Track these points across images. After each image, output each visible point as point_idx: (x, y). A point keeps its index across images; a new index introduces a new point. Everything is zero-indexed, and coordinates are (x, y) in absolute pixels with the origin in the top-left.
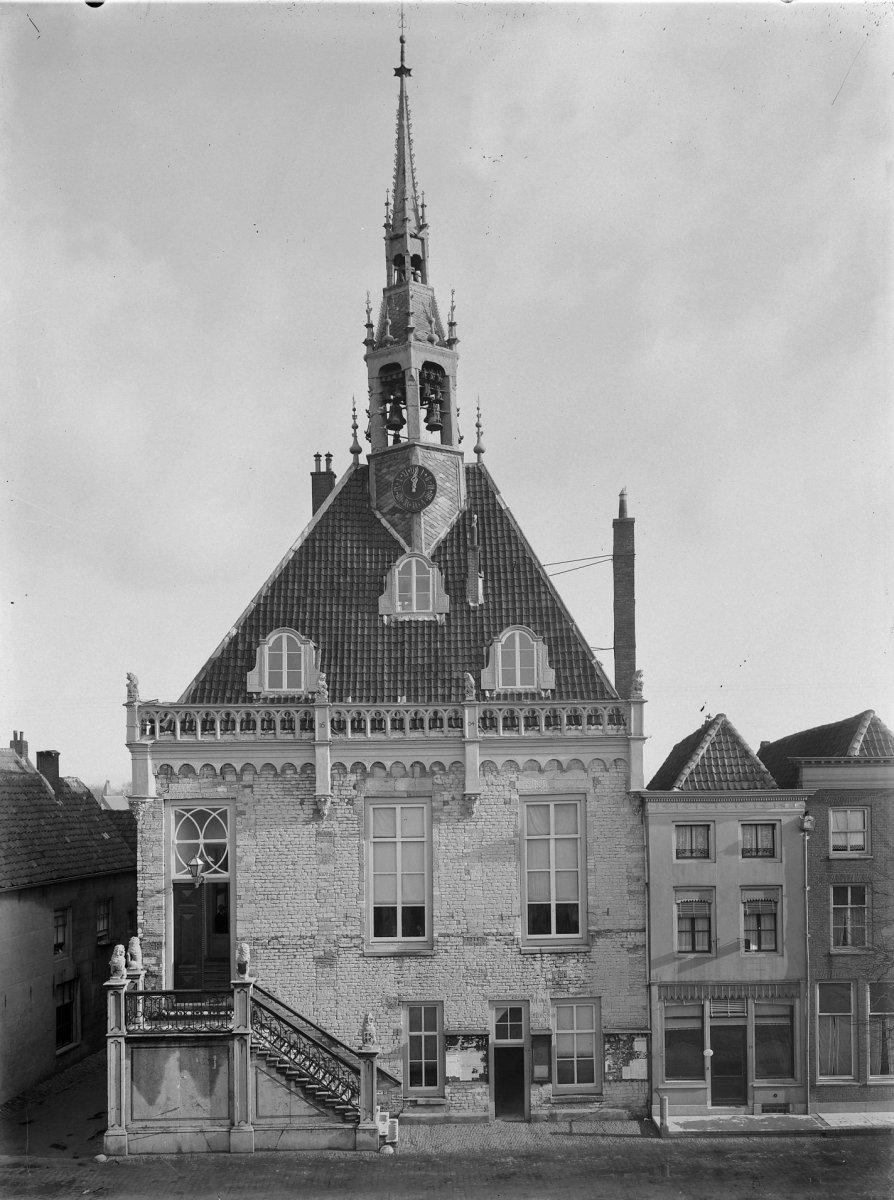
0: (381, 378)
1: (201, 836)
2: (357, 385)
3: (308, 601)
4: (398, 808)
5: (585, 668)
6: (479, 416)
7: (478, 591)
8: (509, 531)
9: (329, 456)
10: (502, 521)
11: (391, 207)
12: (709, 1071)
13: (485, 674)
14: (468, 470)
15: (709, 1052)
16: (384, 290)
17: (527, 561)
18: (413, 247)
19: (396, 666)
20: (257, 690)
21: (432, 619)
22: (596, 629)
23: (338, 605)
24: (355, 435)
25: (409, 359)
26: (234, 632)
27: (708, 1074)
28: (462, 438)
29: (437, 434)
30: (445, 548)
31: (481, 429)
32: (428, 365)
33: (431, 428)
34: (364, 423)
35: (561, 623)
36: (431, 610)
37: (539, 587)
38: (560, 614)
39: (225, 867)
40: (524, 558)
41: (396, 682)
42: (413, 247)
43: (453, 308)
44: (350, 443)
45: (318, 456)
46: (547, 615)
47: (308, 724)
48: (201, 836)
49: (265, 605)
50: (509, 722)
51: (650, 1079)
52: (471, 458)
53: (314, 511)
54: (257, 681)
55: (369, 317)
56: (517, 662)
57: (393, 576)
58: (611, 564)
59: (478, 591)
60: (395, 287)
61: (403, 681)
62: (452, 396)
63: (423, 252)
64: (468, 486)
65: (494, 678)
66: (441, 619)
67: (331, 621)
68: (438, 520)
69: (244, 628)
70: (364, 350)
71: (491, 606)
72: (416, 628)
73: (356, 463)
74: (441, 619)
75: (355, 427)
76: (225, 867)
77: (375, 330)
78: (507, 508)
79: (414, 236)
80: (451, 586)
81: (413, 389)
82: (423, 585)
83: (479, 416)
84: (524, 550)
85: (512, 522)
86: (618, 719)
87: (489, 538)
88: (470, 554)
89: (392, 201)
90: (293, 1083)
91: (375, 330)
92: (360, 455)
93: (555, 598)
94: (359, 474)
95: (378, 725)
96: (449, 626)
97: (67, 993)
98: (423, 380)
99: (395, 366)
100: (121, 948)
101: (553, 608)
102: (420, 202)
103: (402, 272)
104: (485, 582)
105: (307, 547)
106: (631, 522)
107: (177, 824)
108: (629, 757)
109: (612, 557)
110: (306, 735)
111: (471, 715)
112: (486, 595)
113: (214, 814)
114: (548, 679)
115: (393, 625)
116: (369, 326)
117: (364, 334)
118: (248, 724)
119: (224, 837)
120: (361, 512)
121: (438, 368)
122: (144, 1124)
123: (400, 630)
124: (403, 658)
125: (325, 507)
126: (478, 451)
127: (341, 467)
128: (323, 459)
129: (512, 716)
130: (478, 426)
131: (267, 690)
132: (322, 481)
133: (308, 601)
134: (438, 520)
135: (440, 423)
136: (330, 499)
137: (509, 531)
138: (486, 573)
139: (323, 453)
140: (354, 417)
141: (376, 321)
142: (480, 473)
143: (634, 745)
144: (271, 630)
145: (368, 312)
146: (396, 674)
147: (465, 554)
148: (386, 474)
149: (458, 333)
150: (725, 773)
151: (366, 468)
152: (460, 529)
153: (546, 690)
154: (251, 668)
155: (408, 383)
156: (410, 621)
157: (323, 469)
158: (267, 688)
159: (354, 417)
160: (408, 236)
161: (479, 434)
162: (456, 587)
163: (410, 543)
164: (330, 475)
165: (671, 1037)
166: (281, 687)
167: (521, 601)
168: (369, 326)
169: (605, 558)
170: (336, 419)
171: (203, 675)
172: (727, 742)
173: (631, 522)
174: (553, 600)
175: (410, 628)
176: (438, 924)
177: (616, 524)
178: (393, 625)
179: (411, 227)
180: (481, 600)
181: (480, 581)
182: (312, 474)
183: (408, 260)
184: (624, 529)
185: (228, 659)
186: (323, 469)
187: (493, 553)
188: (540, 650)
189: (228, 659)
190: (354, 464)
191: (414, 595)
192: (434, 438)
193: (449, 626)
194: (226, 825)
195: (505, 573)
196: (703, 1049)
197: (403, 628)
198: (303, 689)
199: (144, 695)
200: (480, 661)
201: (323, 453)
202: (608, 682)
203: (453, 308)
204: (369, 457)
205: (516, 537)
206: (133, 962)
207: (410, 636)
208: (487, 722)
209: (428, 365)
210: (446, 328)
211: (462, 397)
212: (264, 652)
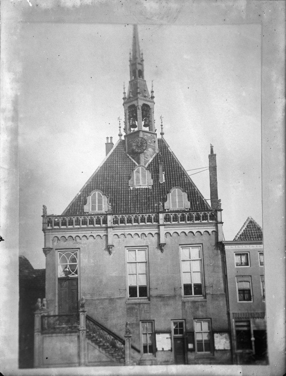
0: (129, 110)
1: (68, 262)
2: (120, 112)
6: (162, 122)
8: (173, 159)
9: (111, 138)
10: (170, 156)
11: (131, 55)
13: (166, 204)
14: (159, 140)
15: (253, 339)
17: (180, 168)
18: (139, 67)
19: (135, 203)
21: (147, 187)
24: (120, 130)
26: (80, 193)
27: (253, 347)
28: (156, 130)
30: (151, 165)
31: (163, 127)
32: (144, 105)
33: (145, 126)
34: (123, 126)
35: (192, 187)
37: (184, 176)
38: (191, 184)
39: (76, 273)
40: (178, 167)
41: (135, 208)
42: (139, 67)
43: (152, 86)
44: (118, 132)
45: (108, 138)
48: (68, 262)
50: (175, 219)
52: (159, 136)
53: (107, 153)
54: (87, 208)
56: (177, 200)
64: (158, 143)
65: (169, 205)
66: (150, 187)
67: (113, 189)
71: (167, 183)
72: (142, 190)
73: (120, 139)
74: (150, 187)
75: (120, 127)
76: (76, 273)
79: (139, 64)
81: (139, 112)
82: (144, 176)
83: (162, 122)
84: (178, 165)
85: (174, 156)
86: (214, 217)
89: (132, 53)
95: (130, 221)
98: (143, 110)
101: (189, 182)
102: (141, 53)
103: (135, 77)
104: (165, 175)
107: (59, 258)
110: (104, 225)
111: (161, 216)
112: (166, 179)
114: (188, 205)
115: (134, 190)
116: (124, 93)
117: (123, 96)
118: (84, 223)
121: (147, 106)
124: (137, 200)
129: (175, 217)
130: (162, 126)
131: (91, 211)
132: (109, 145)
133: (105, 183)
136: (112, 151)
137: (173, 159)
138: (165, 172)
139: (109, 137)
140: (120, 124)
141: (127, 91)
142: (163, 141)
145: (124, 88)
146: (135, 205)
147: (158, 166)
149: (154, 94)
150: (253, 235)
151: (124, 141)
153: (187, 209)
154: (85, 204)
155: (138, 110)
156: (140, 188)
157: (109, 142)
158: (91, 211)
160: (137, 64)
161: (162, 128)
162: (156, 177)
168: (124, 93)
169: (205, 169)
171: (69, 207)
172: (252, 225)
174: (189, 180)
175: (140, 190)
178: (134, 190)
179: (139, 61)
180: (164, 181)
181: (163, 175)
182: (106, 144)
184: (212, 157)
185: (78, 202)
186: (109, 142)
187: (169, 170)
188: (185, 195)
189: (78, 202)
192: (147, 129)
194: (77, 257)
196: (250, 337)
197: (137, 190)
198: (103, 210)
199: (49, 213)
200: (165, 200)
201: (109, 137)
202: (209, 206)
203: (152, 86)
204: (125, 136)
205: (175, 161)
208: (167, 219)
209: (144, 105)
211: (156, 116)
212: (89, 199)
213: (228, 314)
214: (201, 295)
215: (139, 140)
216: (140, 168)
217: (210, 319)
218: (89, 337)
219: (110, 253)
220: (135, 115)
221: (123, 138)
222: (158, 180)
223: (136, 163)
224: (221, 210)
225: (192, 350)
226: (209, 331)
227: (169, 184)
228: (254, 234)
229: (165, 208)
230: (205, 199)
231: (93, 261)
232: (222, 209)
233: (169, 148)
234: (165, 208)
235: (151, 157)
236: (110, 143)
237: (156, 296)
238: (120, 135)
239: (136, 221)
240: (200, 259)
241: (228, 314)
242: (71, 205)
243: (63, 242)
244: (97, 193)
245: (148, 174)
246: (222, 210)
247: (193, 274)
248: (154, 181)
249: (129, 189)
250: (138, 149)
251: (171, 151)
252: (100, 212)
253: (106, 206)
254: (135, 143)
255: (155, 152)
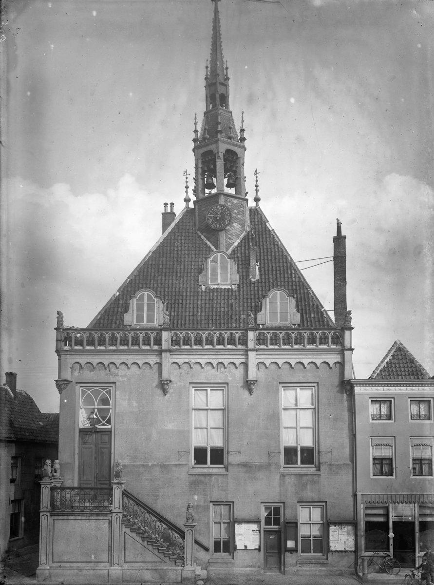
0: (202, 159)
1: (96, 404)
3: (160, 277)
4: (209, 389)
5: (318, 313)
6: (257, 181)
7: (256, 273)
11: (209, 69)
12: (392, 546)
16: (205, 113)
17: (284, 257)
20: (130, 323)
21: (229, 287)
22: (322, 288)
23: (176, 280)
24: (187, 192)
25: (217, 148)
27: (391, 548)
29: (233, 189)
30: (238, 250)
31: (258, 188)
32: (228, 151)
34: (192, 186)
35: (303, 289)
36: (229, 282)
39: (109, 422)
40: (282, 255)
42: (221, 90)
43: (243, 121)
44: (184, 196)
45: (166, 204)
46: (296, 286)
47: (158, 341)
48: (96, 404)
49: (135, 280)
50: (274, 341)
51: (356, 552)
52: (252, 204)
53: (164, 228)
54: (130, 318)
55: (196, 127)
56: (278, 308)
57: (207, 263)
58: (332, 263)
59: (256, 273)
60: (211, 111)
61: (212, 320)
62: (242, 169)
63: (227, 92)
65: (265, 317)
66: (235, 287)
68: (235, 235)
69: (123, 291)
70: (192, 145)
72: (221, 292)
73: (187, 207)
74: (235, 287)
75: (187, 187)
76: (109, 422)
77: (199, 134)
78: (273, 230)
80: (241, 270)
81: (220, 164)
83: (257, 181)
84: (282, 251)
86: (339, 340)
87: (262, 243)
88: (252, 252)
89: (209, 66)
90: (146, 541)
91: (199, 134)
92: (189, 203)
93: (300, 276)
94: (189, 212)
95: (199, 342)
96: (239, 291)
97: (17, 508)
99: (210, 152)
100: (49, 462)
101: (299, 282)
105: (159, 250)
106: (345, 237)
108: (344, 361)
109: (332, 259)
110: (156, 347)
111: (251, 335)
112: (261, 275)
113: (104, 422)
114: (297, 318)
115: (208, 291)
116: (196, 131)
117: (193, 136)
118: (124, 342)
119: (109, 405)
120: (192, 233)
121: (234, 153)
122: (59, 564)
123: (211, 293)
125: (169, 229)
126: (257, 200)
127: (179, 209)
128: (169, 206)
132: (168, 217)
134: (235, 235)
135: (236, 181)
136: (172, 225)
139: (169, 203)
140: (187, 182)
141: (199, 128)
142: (258, 212)
143: (347, 353)
144: (139, 290)
145: (196, 124)
148: (204, 211)
149: (246, 135)
152: (246, 240)
153: (295, 325)
155: (217, 160)
157: (169, 210)
158: (135, 323)
159: (187, 182)
161: (257, 191)
162: (244, 266)
163: (217, 247)
164: (173, 214)
165: (370, 526)
166: (143, 322)
167: (281, 278)
168: (196, 131)
170: (179, 193)
173: (345, 237)
174: (299, 277)
175: (217, 292)
176: (233, 458)
177: (335, 239)
180: (258, 278)
181: (257, 267)
182: (162, 214)
183: (218, 96)
184: (339, 241)
186: (169, 210)
188: (291, 303)
190: (186, 207)
191: (221, 274)
192: (232, 191)
193: (239, 291)
194: (110, 398)
195: (272, 263)
197: (213, 292)
198: (155, 323)
199: (67, 324)
200: (258, 309)
201: (169, 203)
202: (331, 320)
204: (195, 202)
205: (278, 245)
206: (55, 474)
207: (217, 296)
208: (260, 340)
209: (228, 151)
210: (238, 132)
212: (133, 304)
213: (355, 496)
214: (313, 466)
215: (218, 209)
216: (219, 255)
217: (324, 504)
218: (127, 523)
219: (165, 392)
220: (212, 167)
221: (191, 205)
222: (248, 275)
223: (213, 247)
224: (351, 329)
225: (294, 551)
226: (322, 522)
227: (263, 238)
228: (403, 369)
229: (258, 323)
230: (325, 310)
231: (137, 405)
232: (353, 326)
233: (267, 224)
234: (258, 323)
235: (238, 238)
236: (169, 213)
237: (239, 465)
238: (187, 200)
239: (210, 341)
240: (313, 407)
241: (355, 496)
242: (103, 312)
243: (89, 372)
244: (146, 293)
245: (231, 265)
246: (353, 328)
247: (301, 432)
248: (242, 278)
249: (200, 290)
250: (216, 224)
251: (271, 229)
252: (150, 325)
253: (159, 315)
254: (211, 214)
255: (244, 230)
